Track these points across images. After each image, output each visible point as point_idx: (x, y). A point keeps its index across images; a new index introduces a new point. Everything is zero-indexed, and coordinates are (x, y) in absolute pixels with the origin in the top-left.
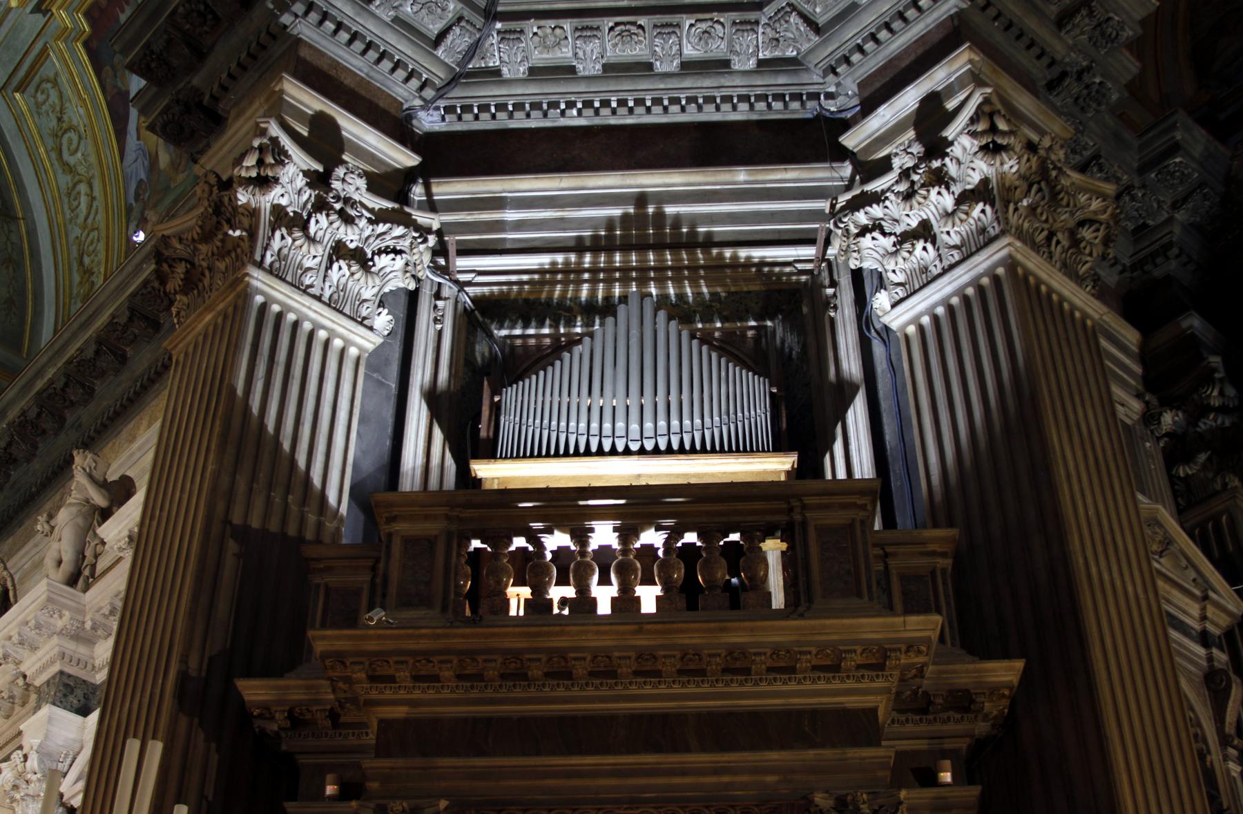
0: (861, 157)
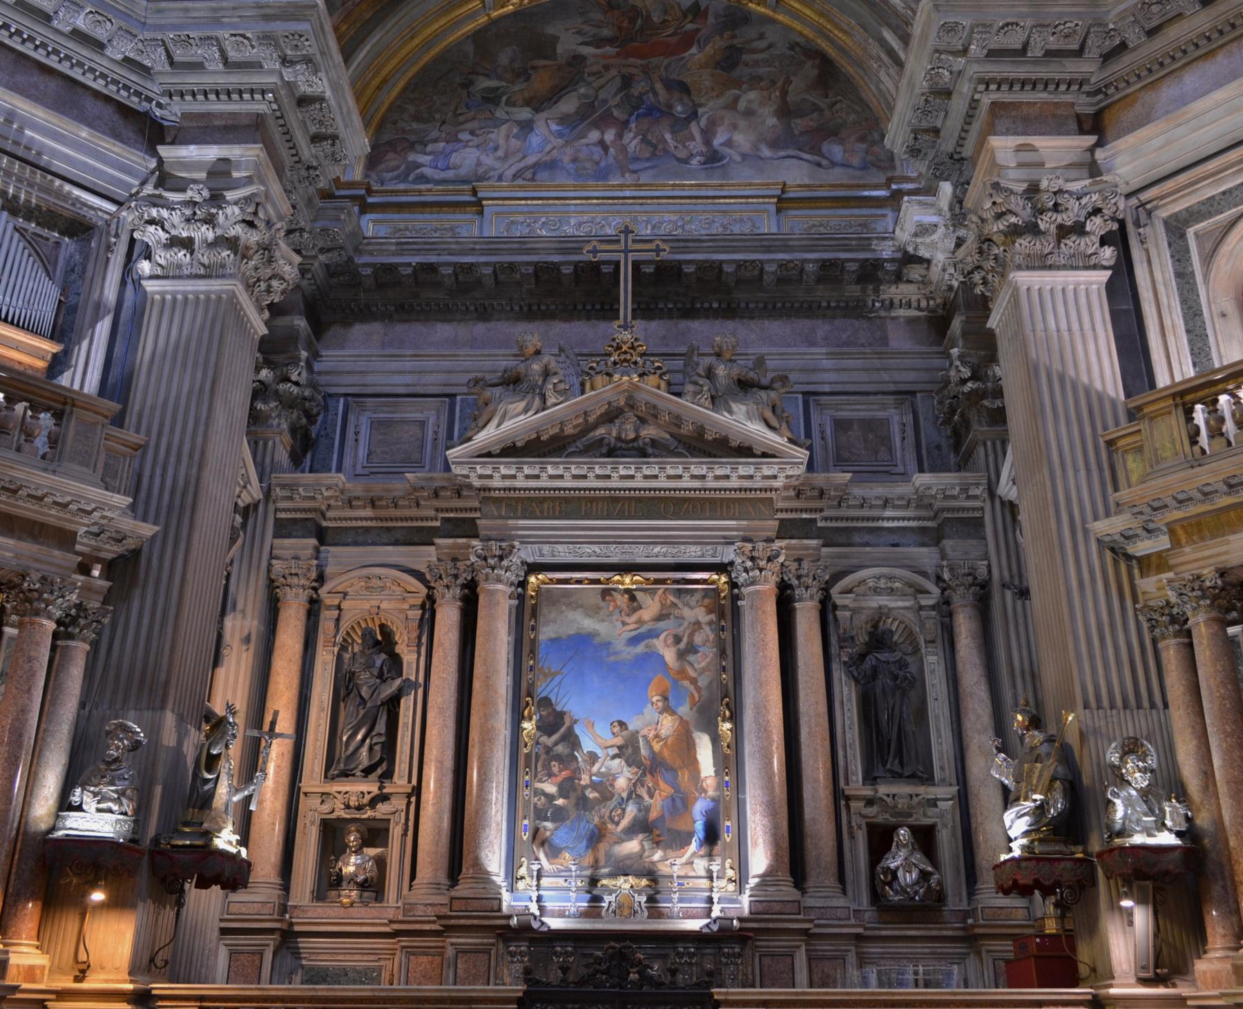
0: (167, 168)
